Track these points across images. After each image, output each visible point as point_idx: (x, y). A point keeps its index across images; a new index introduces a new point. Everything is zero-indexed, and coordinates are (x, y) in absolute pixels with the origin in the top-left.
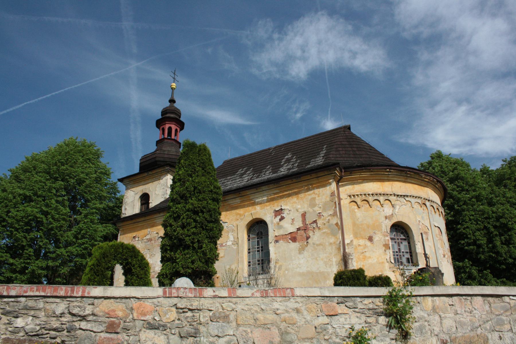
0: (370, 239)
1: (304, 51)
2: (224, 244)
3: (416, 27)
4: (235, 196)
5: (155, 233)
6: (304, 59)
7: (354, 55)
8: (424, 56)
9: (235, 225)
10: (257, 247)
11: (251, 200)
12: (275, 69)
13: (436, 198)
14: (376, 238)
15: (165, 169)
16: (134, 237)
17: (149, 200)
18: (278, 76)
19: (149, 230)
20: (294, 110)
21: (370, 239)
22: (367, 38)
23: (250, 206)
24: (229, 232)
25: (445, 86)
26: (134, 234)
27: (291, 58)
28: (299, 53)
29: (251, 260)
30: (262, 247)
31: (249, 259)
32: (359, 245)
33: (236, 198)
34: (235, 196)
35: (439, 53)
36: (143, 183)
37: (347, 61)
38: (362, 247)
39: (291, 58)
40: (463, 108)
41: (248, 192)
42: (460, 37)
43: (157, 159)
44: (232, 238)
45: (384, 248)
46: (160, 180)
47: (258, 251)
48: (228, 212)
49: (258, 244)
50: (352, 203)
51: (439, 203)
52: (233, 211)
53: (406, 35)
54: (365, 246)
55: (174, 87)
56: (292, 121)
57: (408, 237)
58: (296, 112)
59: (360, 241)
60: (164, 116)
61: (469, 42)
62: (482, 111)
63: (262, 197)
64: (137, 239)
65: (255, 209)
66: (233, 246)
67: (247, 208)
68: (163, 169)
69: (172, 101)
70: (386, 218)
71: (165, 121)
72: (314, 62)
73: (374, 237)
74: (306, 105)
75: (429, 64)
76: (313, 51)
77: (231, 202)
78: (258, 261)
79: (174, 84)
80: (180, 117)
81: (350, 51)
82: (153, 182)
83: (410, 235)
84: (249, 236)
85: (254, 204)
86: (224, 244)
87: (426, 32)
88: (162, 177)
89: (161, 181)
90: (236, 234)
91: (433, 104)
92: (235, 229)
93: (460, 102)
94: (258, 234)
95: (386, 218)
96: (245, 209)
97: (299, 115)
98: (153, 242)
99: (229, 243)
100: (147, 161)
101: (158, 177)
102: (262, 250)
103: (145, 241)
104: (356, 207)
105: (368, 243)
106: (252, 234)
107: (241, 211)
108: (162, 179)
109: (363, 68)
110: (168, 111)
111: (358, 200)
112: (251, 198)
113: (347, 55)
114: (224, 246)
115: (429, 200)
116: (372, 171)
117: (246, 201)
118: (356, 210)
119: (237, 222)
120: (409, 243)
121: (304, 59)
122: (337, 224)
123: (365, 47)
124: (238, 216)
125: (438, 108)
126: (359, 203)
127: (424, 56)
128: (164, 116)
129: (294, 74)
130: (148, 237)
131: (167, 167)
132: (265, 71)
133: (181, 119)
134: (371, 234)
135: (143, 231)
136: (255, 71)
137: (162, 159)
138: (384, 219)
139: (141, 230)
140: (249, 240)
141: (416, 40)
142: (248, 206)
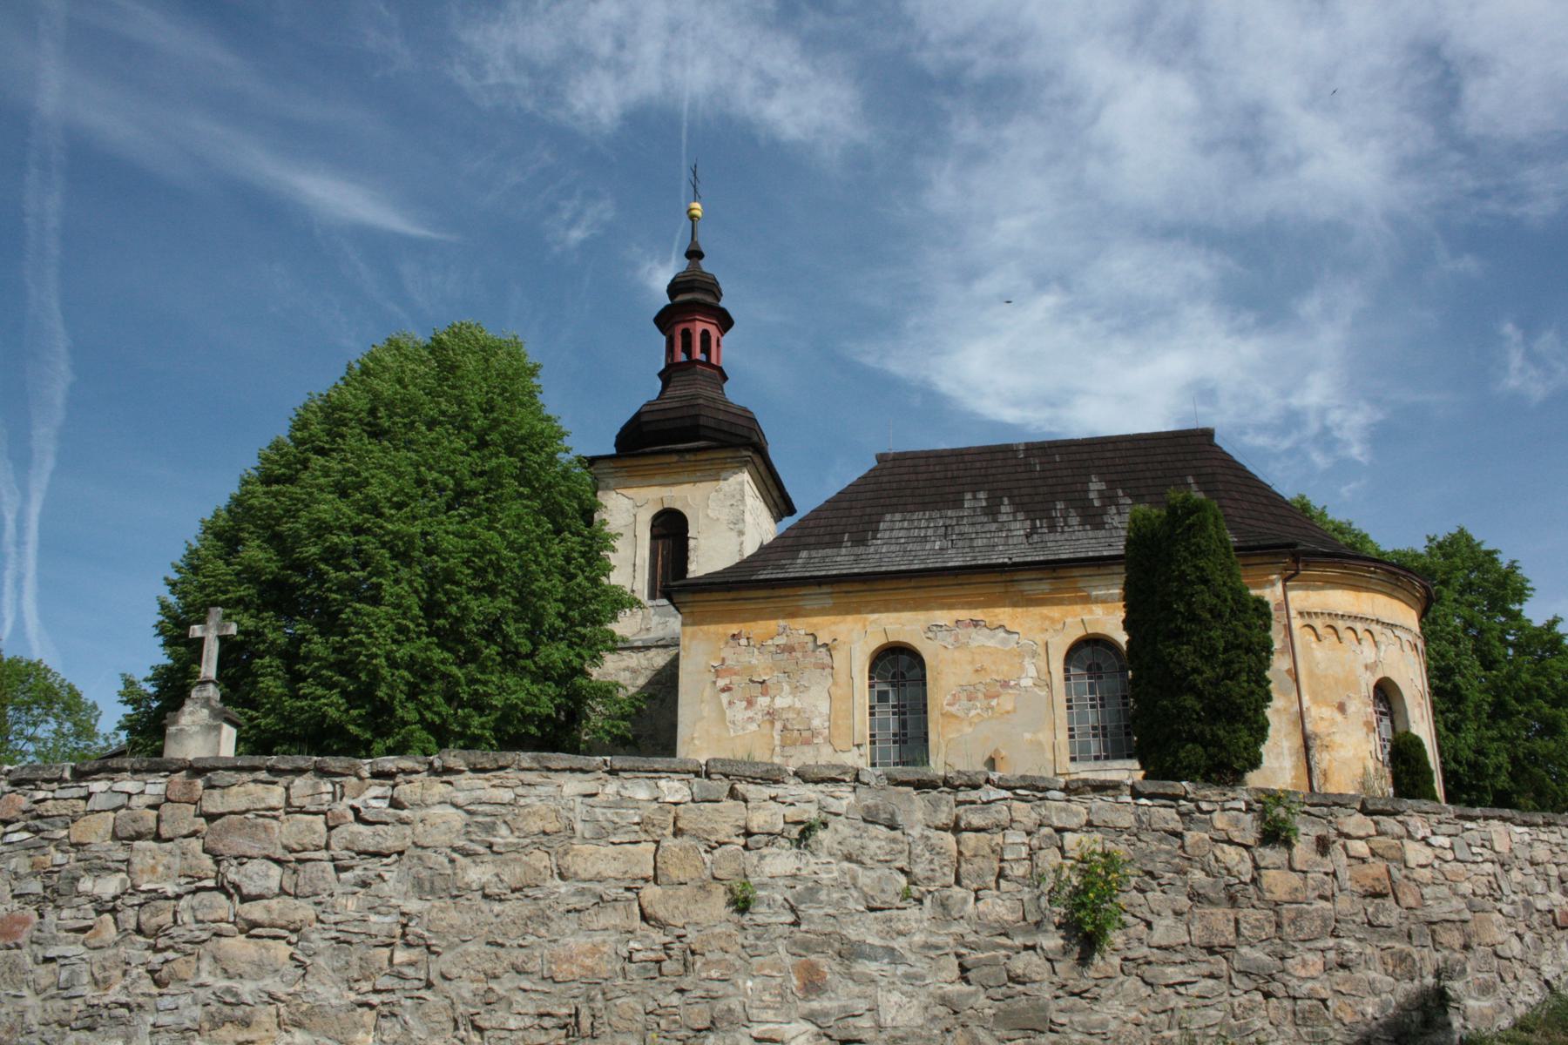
0: (1342, 708)
1: (620, 45)
2: (1012, 683)
3: (959, 42)
4: (1040, 576)
5: (803, 632)
6: (619, 69)
7: (769, 86)
8: (968, 131)
9: (1040, 643)
10: (1088, 696)
11: (1079, 589)
12: (525, 81)
13: (1408, 617)
14: (1352, 708)
15: (738, 454)
16: (734, 635)
17: (687, 531)
18: (529, 104)
19: (782, 623)
20: (566, 216)
21: (1342, 708)
22: (814, 45)
23: (1076, 603)
24: (1024, 657)
25: (1011, 229)
26: (734, 629)
27: (578, 57)
28: (605, 48)
29: (1075, 726)
30: (1102, 699)
31: (1070, 720)
32: (1322, 718)
33: (1041, 579)
34: (1040, 576)
35: (1010, 132)
36: (659, 479)
37: (745, 98)
38: (1327, 724)
39: (578, 57)
40: (1049, 300)
41: (1076, 572)
42: (1070, 101)
43: (702, 421)
44: (1032, 672)
45: (1365, 730)
46: (718, 480)
47: (1093, 706)
48: (1020, 610)
49: (1092, 691)
50: (1307, 629)
51: (1415, 627)
52: (1031, 609)
53: (927, 59)
54: (1333, 722)
55: (698, 213)
56: (557, 249)
57: (1390, 709)
58: (572, 223)
59: (1324, 709)
60: (680, 298)
61: (1094, 118)
62: (1098, 319)
63: (1108, 587)
64: (743, 642)
65: (1091, 612)
66: (1036, 689)
67: (1069, 608)
68: (731, 455)
69: (694, 254)
70: (1366, 667)
71: (694, 312)
72: (646, 82)
73: (1348, 704)
74: (605, 210)
75: (976, 156)
76: (650, 50)
77: (1026, 587)
78: (1094, 728)
79: (697, 205)
80: (719, 300)
81: (760, 73)
82: (695, 482)
83: (1395, 706)
84: (1066, 670)
85: (1087, 600)
86: (1012, 683)
87: (983, 65)
88: (724, 475)
89: (722, 483)
90: (1043, 665)
91: (970, 274)
92: (1041, 651)
93: (1042, 283)
94: (1089, 669)
95: (1366, 667)
96: (1064, 608)
97: (576, 235)
98: (799, 655)
99: (1026, 682)
100: (669, 419)
101: (712, 472)
102: (1102, 706)
103: (773, 649)
104: (1313, 638)
105: (1338, 717)
106: (1075, 666)
107: (1054, 612)
108: (725, 479)
109: (791, 130)
110: (697, 284)
111: (1318, 623)
112: (1080, 585)
113: (747, 83)
114: (1011, 688)
115: (1378, 622)
116: (1345, 568)
117: (1067, 590)
118: (1314, 645)
119: (1046, 637)
120: (1392, 722)
121: (619, 69)
122: (1288, 671)
123: (802, 70)
124: (1047, 622)
125: (987, 286)
126: (1320, 630)
127: (968, 131)
128: (680, 298)
129: (580, 106)
130: (781, 640)
131: (747, 450)
132: (492, 80)
133: (723, 304)
134: (1343, 698)
135: (761, 623)
136: (460, 74)
137: (712, 423)
138: (1363, 669)
139: (754, 619)
140: (1067, 679)
141: (952, 82)
142: (1072, 602)
